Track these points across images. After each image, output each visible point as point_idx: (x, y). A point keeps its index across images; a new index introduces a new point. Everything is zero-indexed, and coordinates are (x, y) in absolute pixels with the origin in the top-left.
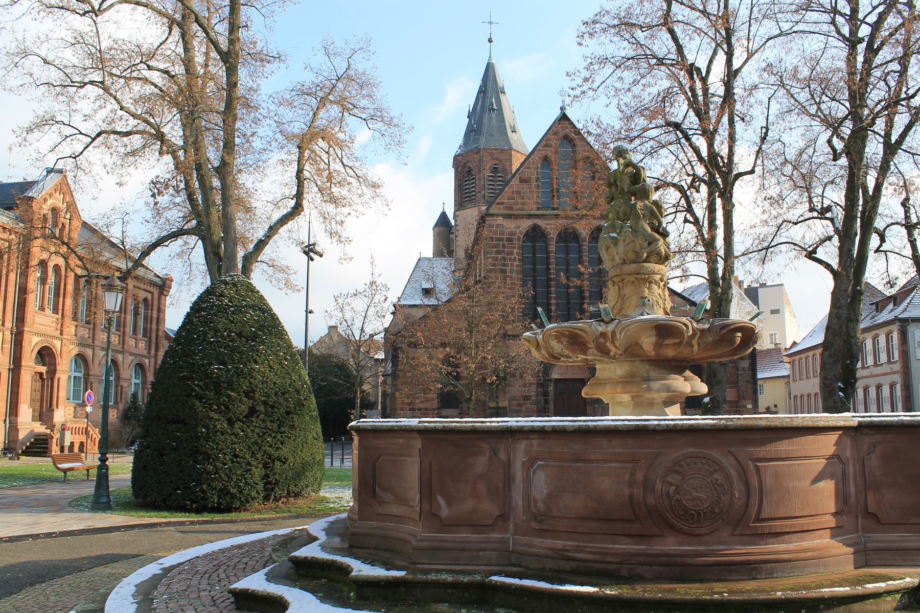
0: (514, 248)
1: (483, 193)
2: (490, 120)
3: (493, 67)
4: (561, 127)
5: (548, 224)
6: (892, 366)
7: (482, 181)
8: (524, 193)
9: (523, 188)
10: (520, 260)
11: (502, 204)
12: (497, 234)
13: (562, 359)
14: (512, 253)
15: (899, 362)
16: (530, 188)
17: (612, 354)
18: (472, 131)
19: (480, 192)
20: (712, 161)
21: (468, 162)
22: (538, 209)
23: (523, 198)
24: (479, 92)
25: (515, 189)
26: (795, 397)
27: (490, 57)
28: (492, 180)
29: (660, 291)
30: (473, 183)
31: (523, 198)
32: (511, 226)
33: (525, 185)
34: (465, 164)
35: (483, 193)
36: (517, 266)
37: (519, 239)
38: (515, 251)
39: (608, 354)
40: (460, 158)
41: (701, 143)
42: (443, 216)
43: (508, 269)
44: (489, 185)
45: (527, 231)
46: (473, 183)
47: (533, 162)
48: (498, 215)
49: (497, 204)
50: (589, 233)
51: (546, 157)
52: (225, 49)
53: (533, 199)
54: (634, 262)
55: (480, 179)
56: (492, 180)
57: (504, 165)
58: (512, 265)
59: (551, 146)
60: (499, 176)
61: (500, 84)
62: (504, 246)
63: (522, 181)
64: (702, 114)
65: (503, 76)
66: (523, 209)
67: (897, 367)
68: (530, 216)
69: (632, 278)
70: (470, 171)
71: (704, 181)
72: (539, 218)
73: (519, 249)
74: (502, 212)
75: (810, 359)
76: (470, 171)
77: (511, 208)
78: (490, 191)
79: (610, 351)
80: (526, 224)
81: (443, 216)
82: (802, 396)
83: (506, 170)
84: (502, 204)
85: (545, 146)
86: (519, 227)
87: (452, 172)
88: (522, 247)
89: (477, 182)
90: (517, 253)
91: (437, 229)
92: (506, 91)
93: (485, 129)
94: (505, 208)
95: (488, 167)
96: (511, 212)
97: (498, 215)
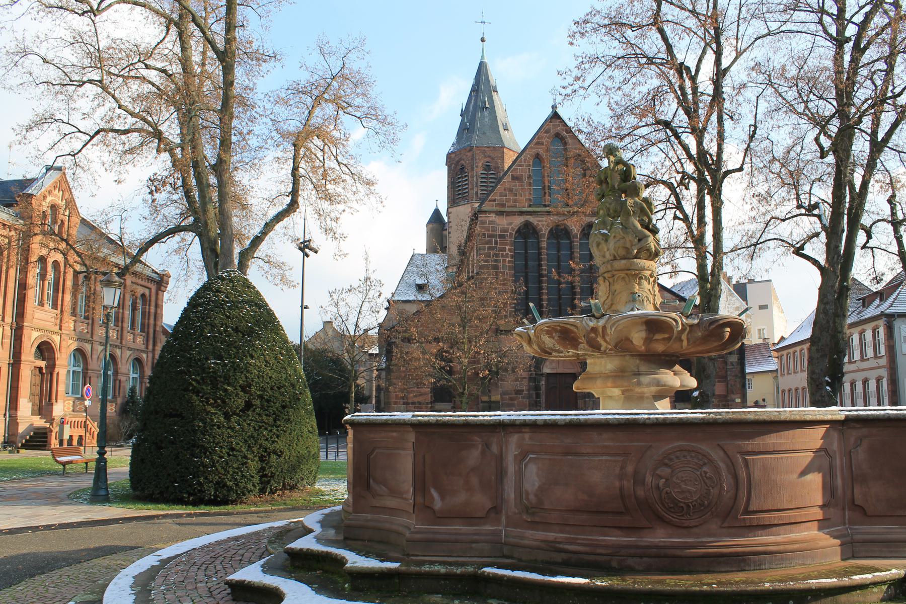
0: (507, 244)
1: (475, 190)
2: (483, 118)
3: (486, 66)
4: (553, 125)
5: (539, 221)
6: (878, 360)
7: (475, 179)
8: (516, 190)
9: (515, 186)
10: (512, 256)
11: (494, 201)
12: (489, 231)
13: (553, 354)
14: (504, 250)
15: (885, 357)
16: (522, 185)
17: (602, 349)
18: (465, 129)
19: (473, 189)
20: (701, 158)
21: (461, 159)
22: (530, 206)
23: (515, 195)
24: (472, 91)
25: (507, 186)
26: (783, 391)
27: (483, 56)
28: (485, 178)
29: (650, 287)
30: (466, 180)
31: (515, 195)
32: (503, 222)
33: (517, 182)
34: (458, 162)
35: (475, 190)
36: (509, 262)
37: (511, 236)
38: (507, 248)
39: (599, 349)
40: (453, 156)
41: (691, 141)
42: (437, 213)
43: (500, 265)
44: (482, 182)
45: (519, 228)
46: (466, 180)
47: (525, 160)
48: (490, 212)
49: (490, 201)
50: (580, 230)
51: (538, 154)
52: (222, 48)
53: (525, 196)
54: (624, 258)
55: (473, 177)
56: (485, 178)
57: (496, 163)
58: (504, 261)
59: (542, 144)
60: (492, 174)
61: (492, 83)
62: (496, 243)
63: (514, 178)
64: (691, 113)
65: (496, 75)
66: (515, 206)
67: (883, 362)
68: (522, 213)
69: (622, 274)
70: (462, 169)
71: (693, 179)
72: (531, 215)
73: (511, 245)
74: (495, 208)
75: (798, 354)
76: (462, 169)
77: (503, 205)
78: (482, 188)
79: (601, 346)
80: (518, 221)
81: (437, 213)
82: (790, 390)
83: (498, 168)
84: (494, 201)
85: (537, 143)
86: (511, 224)
87: (445, 169)
88: (514, 244)
89: (470, 179)
90: (509, 249)
91: (431, 226)
92: (498, 89)
93: (478, 127)
94: (497, 205)
95: (480, 165)
96: (503, 209)
97: (490, 212)
